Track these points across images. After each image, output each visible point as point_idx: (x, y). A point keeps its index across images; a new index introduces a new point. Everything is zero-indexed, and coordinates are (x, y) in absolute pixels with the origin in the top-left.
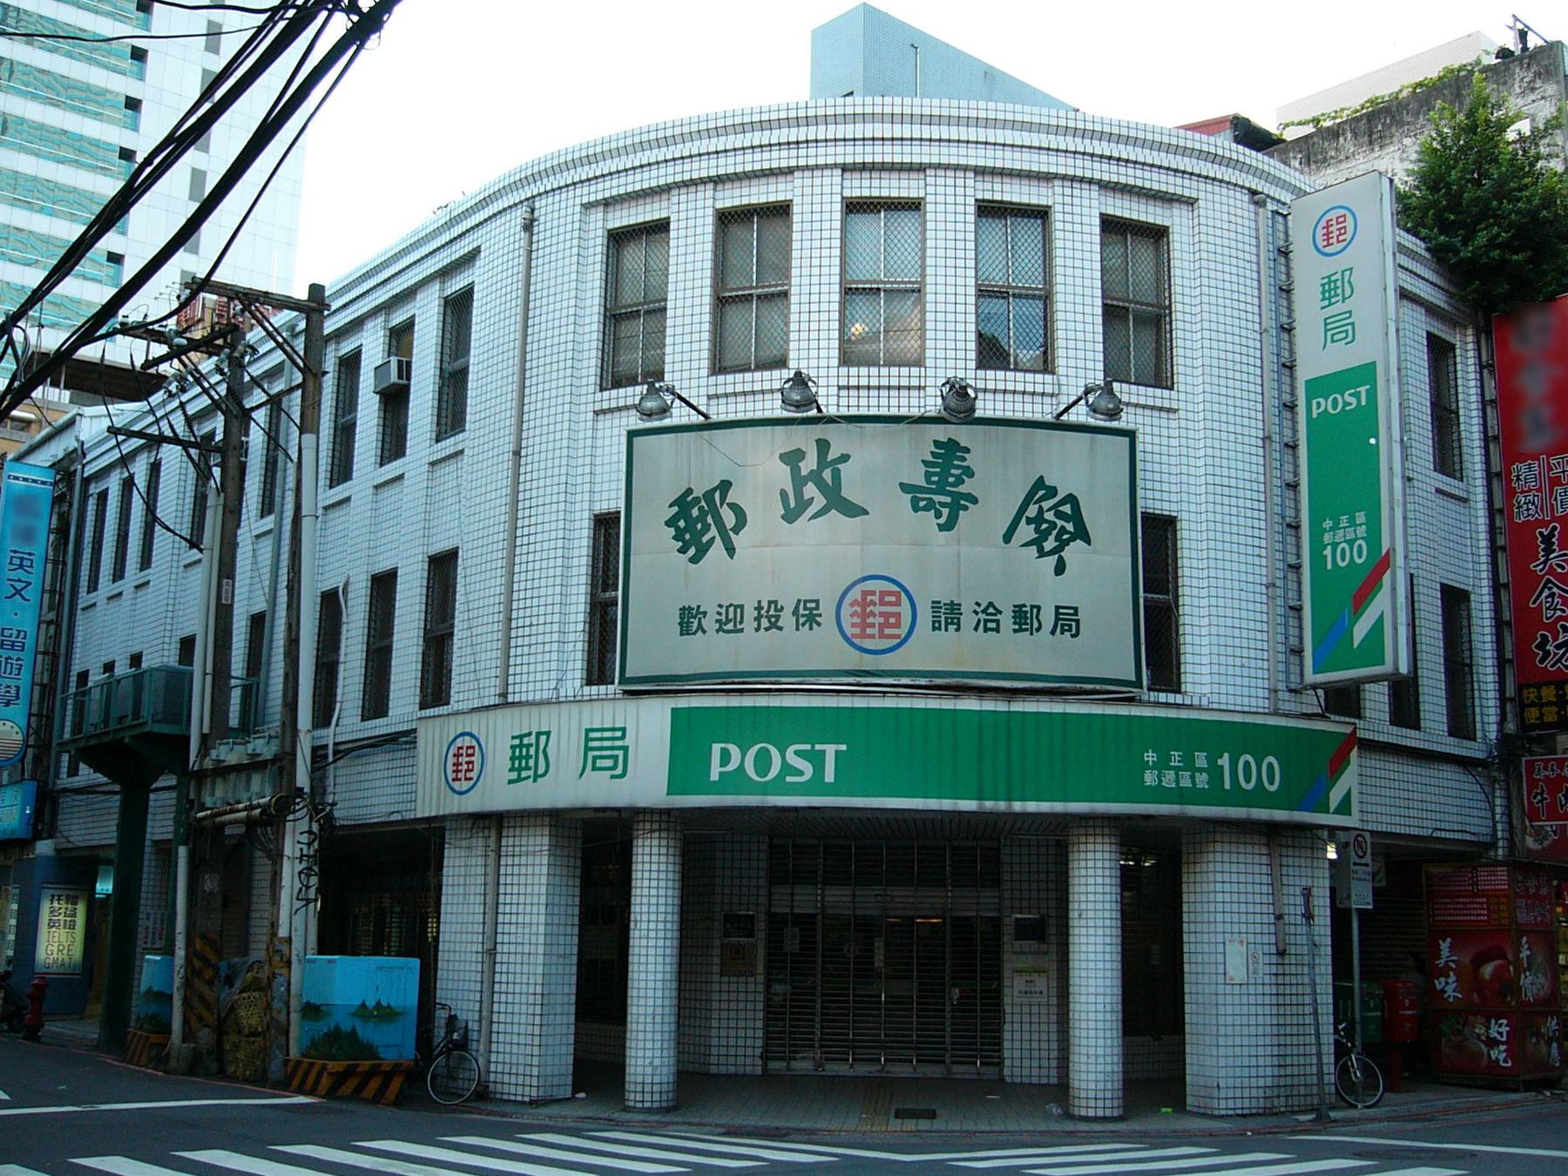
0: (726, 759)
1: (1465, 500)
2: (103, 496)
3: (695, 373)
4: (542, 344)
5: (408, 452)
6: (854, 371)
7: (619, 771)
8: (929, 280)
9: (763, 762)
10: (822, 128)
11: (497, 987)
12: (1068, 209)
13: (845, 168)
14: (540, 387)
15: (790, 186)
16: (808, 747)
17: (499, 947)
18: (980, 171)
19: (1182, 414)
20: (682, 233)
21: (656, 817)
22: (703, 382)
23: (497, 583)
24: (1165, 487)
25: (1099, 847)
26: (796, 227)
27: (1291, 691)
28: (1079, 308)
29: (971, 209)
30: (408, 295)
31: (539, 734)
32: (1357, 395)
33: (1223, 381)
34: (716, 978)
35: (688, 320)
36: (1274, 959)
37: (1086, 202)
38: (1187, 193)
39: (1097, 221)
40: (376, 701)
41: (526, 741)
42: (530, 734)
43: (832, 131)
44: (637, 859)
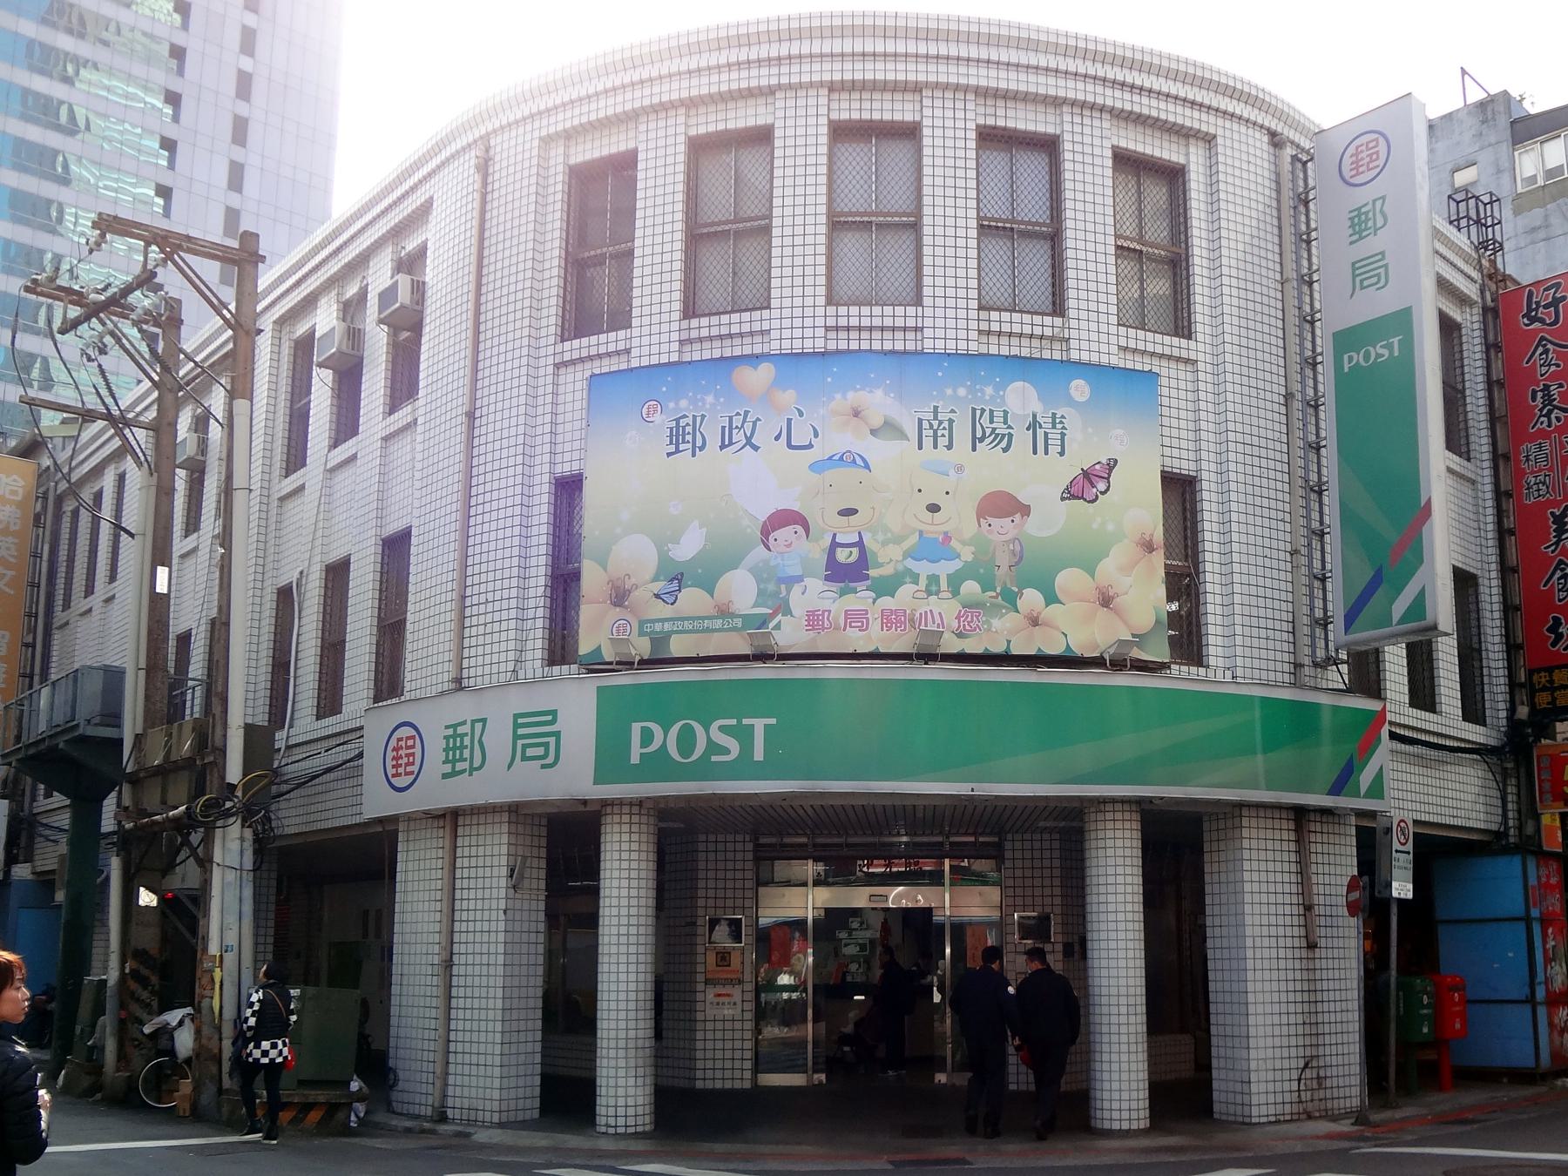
0: (650, 737)
1: (1473, 482)
2: (98, 497)
3: (665, 317)
4: (498, 293)
6: (843, 310)
7: (550, 760)
8: (927, 210)
11: (454, 1002)
12: (1078, 138)
13: (832, 87)
15: (770, 109)
16: (734, 722)
17: (455, 958)
18: (983, 93)
21: (626, 809)
22: (675, 326)
27: (1316, 665)
29: (972, 135)
30: (363, 260)
31: (473, 722)
32: (1389, 347)
35: (657, 259)
36: (1304, 953)
38: (1204, 128)
39: (1109, 153)
40: (330, 702)
41: (460, 730)
42: (464, 723)
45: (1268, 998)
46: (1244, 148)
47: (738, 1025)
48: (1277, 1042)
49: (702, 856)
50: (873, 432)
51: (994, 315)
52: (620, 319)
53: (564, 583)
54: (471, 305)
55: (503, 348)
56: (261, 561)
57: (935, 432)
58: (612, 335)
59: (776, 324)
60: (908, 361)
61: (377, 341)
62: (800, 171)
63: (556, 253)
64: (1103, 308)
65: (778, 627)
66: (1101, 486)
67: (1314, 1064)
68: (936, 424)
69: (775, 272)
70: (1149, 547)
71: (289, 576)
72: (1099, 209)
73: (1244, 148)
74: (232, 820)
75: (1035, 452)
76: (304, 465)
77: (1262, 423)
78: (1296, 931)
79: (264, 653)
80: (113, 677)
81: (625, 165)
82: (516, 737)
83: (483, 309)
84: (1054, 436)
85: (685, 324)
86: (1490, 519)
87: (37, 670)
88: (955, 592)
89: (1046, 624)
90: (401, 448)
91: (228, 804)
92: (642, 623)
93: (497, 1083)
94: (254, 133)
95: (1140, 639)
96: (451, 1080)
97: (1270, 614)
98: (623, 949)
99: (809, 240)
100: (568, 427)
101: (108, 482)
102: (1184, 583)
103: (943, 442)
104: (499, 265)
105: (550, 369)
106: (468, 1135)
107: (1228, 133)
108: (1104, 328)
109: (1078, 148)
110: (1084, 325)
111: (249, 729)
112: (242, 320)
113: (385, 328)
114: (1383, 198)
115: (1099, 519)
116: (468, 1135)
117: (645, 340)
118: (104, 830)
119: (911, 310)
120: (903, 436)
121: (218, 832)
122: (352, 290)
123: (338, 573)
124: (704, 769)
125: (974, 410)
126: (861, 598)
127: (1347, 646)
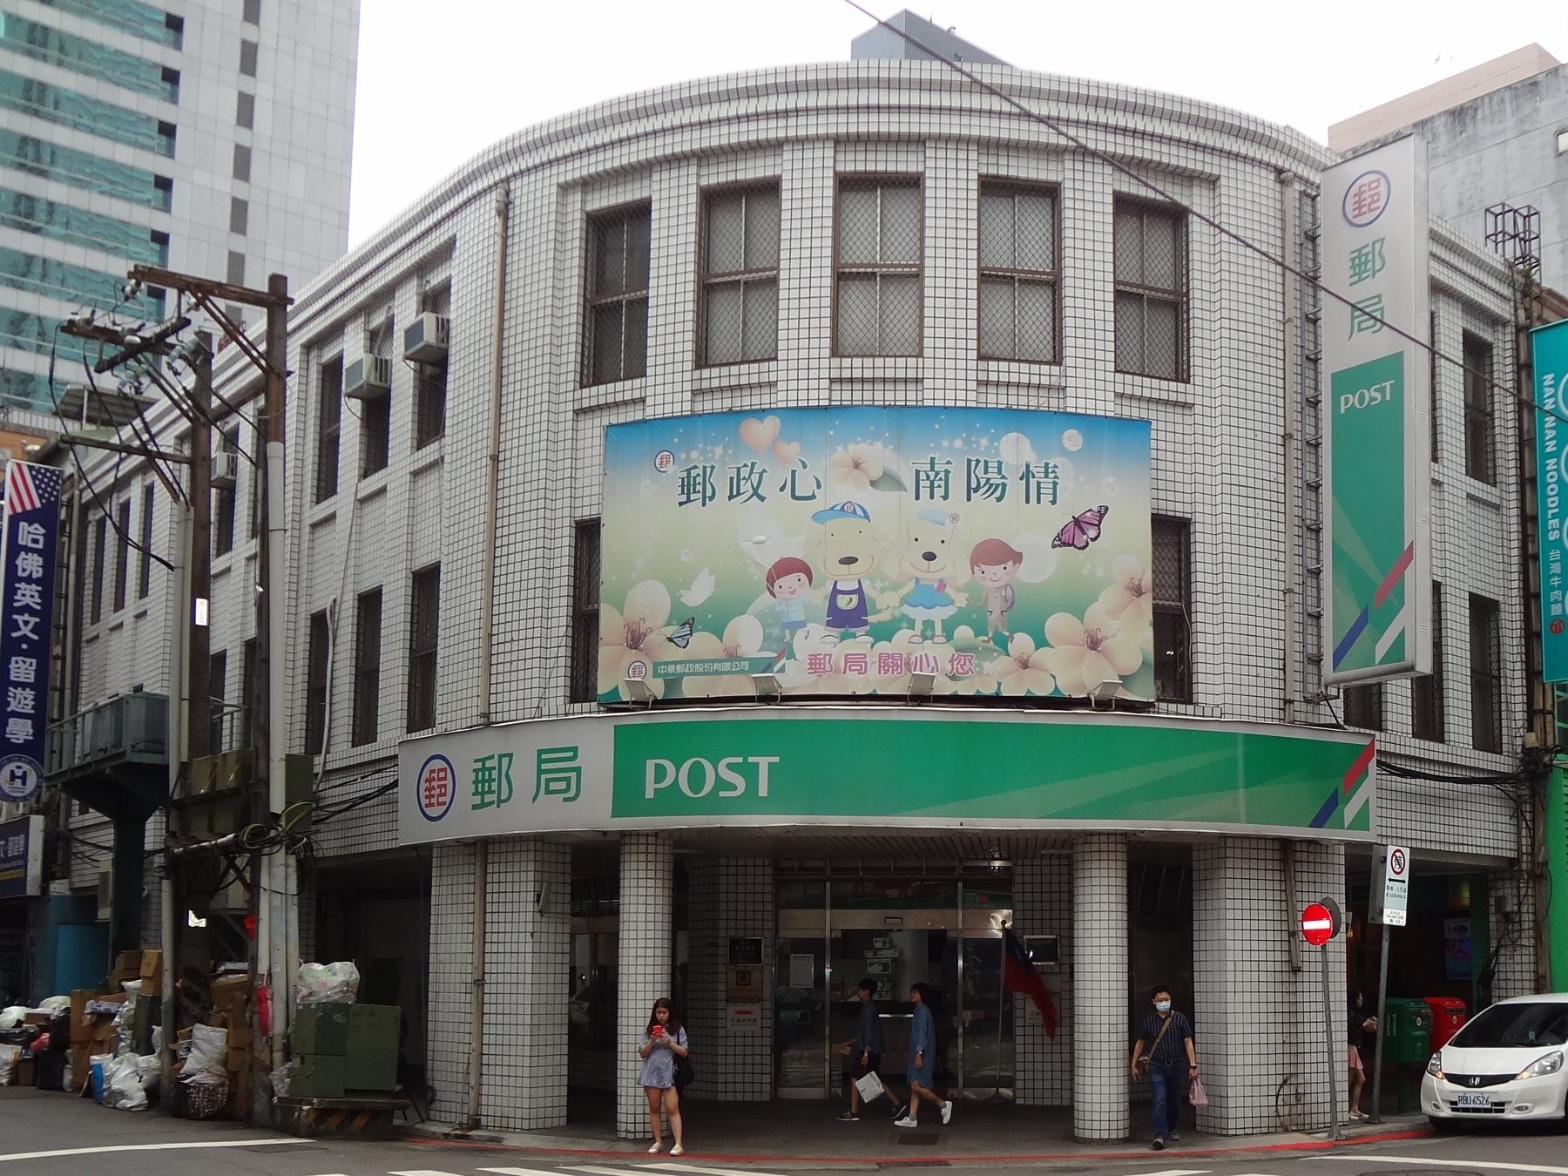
1: (1497, 507)
2: (125, 508)
3: (678, 367)
5: (390, 462)
6: (846, 362)
7: (572, 794)
8: (928, 262)
9: (696, 777)
10: (813, 95)
12: (1079, 185)
14: (518, 386)
15: (778, 161)
16: (740, 760)
19: (1198, 409)
20: (665, 214)
21: (643, 840)
22: (688, 376)
23: (477, 597)
24: (1179, 487)
25: (1104, 873)
26: (785, 205)
27: (1307, 701)
28: (1089, 294)
29: (974, 185)
30: (386, 294)
31: (501, 756)
32: (1382, 390)
33: (1242, 374)
34: (722, 1004)
35: (671, 309)
37: (1098, 178)
38: (1208, 169)
39: (1110, 199)
40: (365, 730)
41: (488, 764)
42: (492, 757)
43: (823, 99)
44: (625, 883)
45: (1247, 1018)
46: (1249, 187)
47: (757, 1041)
48: (1256, 1060)
49: (723, 879)
50: (873, 483)
51: (993, 365)
52: (637, 369)
53: (585, 624)
54: (494, 349)
55: (524, 393)
56: (294, 587)
57: (932, 483)
58: (628, 383)
59: (782, 376)
60: (909, 418)
61: (404, 379)
62: (807, 223)
63: (575, 300)
64: (1100, 355)
65: (782, 670)
66: (1092, 533)
67: (1293, 1080)
68: (932, 475)
69: (782, 325)
70: (1138, 591)
71: (321, 603)
72: (1099, 256)
73: (1249, 187)
74: (276, 848)
75: (1028, 501)
76: (334, 492)
77: (1259, 464)
78: (1278, 956)
79: (299, 687)
80: (157, 705)
81: (640, 212)
82: (540, 772)
83: (505, 353)
84: (1047, 486)
85: (697, 374)
86: (1515, 544)
87: (68, 684)
88: (949, 638)
89: (1036, 667)
90: (429, 483)
91: (273, 833)
92: (656, 665)
93: (526, 1092)
94: (264, 61)
95: (1126, 680)
96: (485, 1090)
97: (1260, 652)
98: (641, 969)
99: (815, 292)
100: (588, 471)
101: (135, 493)
102: (1173, 629)
103: (939, 492)
104: (520, 311)
105: (570, 415)
106: (498, 1140)
107: (1233, 174)
108: (1100, 375)
109: (1079, 195)
110: (1081, 372)
111: (290, 759)
112: (273, 364)
113: (412, 364)
114: (1382, 240)
115: (1089, 566)
116: (498, 1140)
117: (660, 389)
118: (148, 847)
119: (912, 362)
120: (899, 485)
121: (265, 860)
122: (378, 319)
123: (370, 603)
124: (713, 804)
125: (969, 461)
126: (860, 643)
127: (1337, 682)
